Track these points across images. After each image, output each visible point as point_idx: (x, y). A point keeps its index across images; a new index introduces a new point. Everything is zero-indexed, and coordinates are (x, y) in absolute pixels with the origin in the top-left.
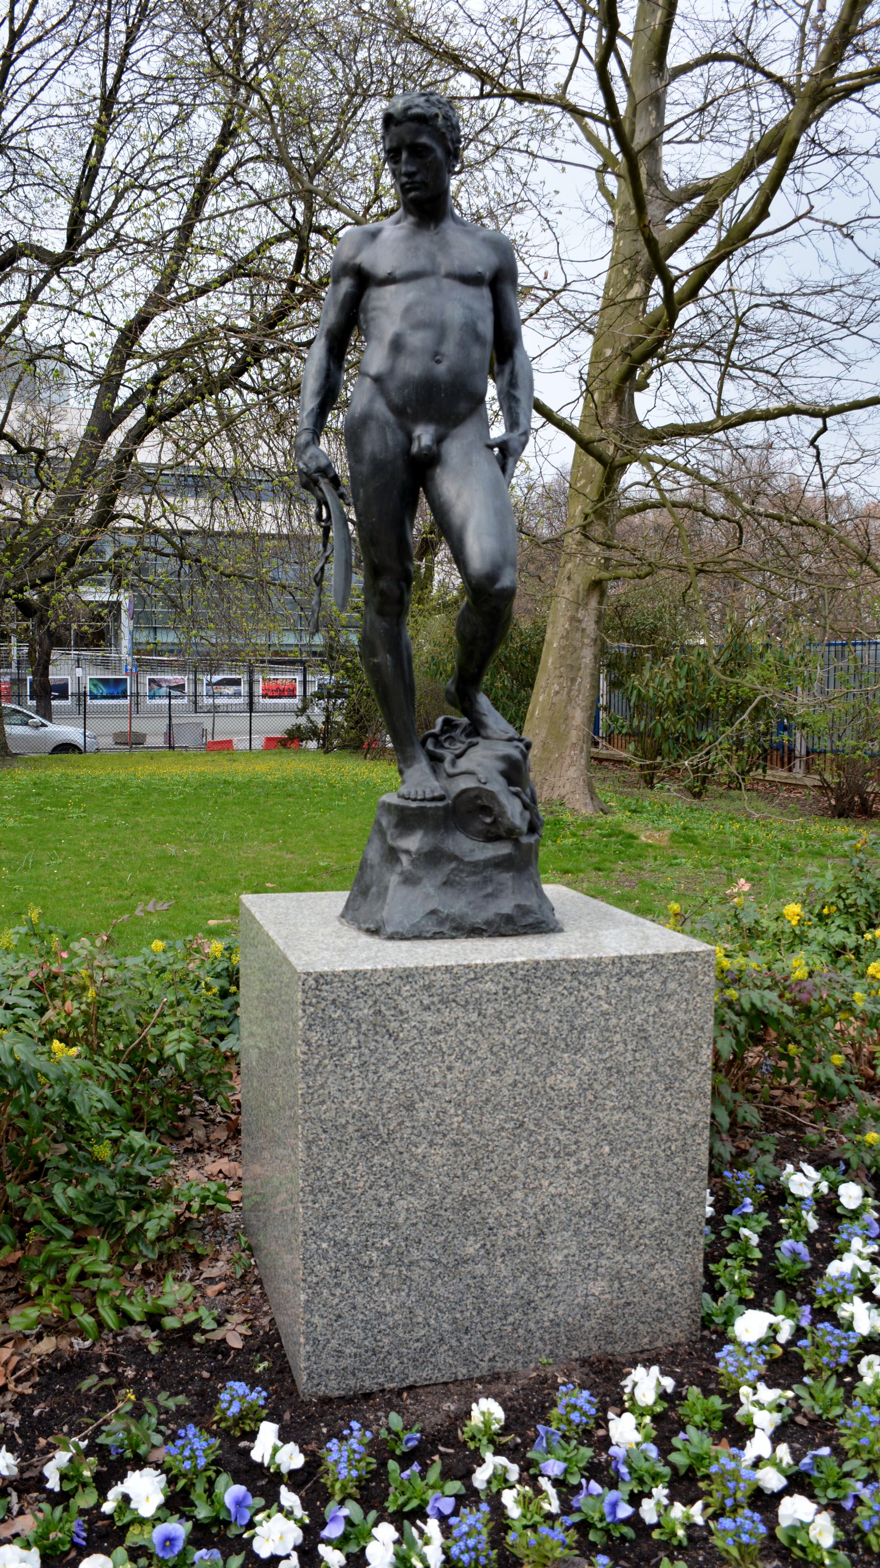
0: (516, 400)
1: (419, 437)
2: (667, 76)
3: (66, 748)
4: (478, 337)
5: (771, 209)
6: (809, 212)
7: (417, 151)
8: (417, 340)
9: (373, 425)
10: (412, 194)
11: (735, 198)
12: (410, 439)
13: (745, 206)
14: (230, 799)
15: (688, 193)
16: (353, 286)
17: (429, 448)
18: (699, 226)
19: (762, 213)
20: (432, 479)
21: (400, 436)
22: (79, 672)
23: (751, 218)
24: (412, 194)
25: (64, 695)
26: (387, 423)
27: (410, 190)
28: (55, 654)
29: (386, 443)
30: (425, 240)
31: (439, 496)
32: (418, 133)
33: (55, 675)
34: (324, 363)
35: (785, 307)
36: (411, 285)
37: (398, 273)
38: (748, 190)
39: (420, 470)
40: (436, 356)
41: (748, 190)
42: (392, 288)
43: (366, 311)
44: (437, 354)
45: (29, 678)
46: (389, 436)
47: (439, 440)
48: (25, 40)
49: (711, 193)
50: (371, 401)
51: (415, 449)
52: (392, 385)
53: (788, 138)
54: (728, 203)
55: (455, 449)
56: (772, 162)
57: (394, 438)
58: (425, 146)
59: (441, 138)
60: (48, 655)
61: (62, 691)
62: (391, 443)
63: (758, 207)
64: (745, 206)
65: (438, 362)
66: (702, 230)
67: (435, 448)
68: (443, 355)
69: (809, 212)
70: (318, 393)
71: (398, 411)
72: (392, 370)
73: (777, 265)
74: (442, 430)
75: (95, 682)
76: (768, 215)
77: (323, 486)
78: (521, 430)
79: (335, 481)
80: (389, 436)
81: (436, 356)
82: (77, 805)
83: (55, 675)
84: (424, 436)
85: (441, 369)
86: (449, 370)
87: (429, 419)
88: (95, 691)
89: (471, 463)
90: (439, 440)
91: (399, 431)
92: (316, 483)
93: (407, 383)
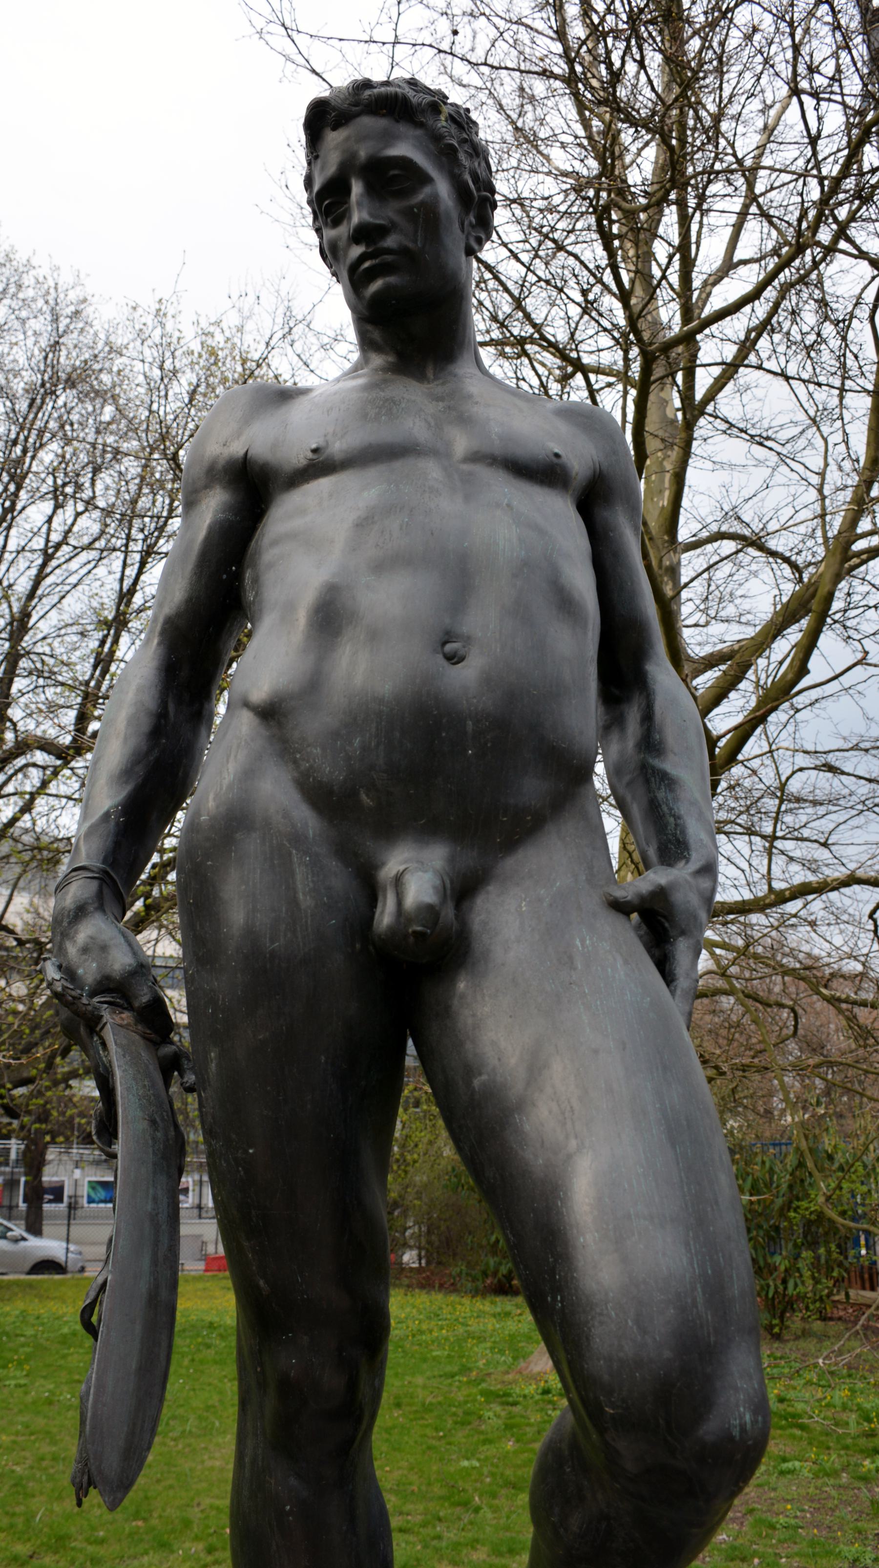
0: (667, 780)
1: (398, 881)
2: (679, 549)
3: (48, 1266)
4: (565, 603)
5: (811, 665)
6: (864, 658)
7: (389, 179)
8: (387, 599)
9: (252, 845)
10: (376, 286)
11: (768, 658)
12: (370, 889)
13: (781, 663)
14: (210, 1353)
15: (710, 662)
16: (228, 508)
17: (430, 912)
18: (729, 691)
19: (802, 670)
20: (446, 1013)
21: (340, 879)
22: (77, 1173)
23: (790, 676)
24: (376, 286)
25: (58, 1198)
26: (297, 839)
27: (371, 275)
28: (51, 1154)
29: (294, 902)
30: (411, 392)
31: (470, 1071)
32: (388, 138)
33: (49, 1177)
34: (150, 701)
35: (831, 769)
36: (373, 473)
37: (338, 448)
38: (783, 647)
39: (411, 979)
40: (449, 647)
41: (782, 647)
42: (323, 484)
43: (254, 565)
44: (448, 637)
45: (23, 1179)
46: (302, 878)
47: (463, 889)
48: (54, 563)
49: (737, 662)
50: (248, 774)
51: (385, 917)
52: (313, 726)
53: (823, 591)
54: (762, 662)
55: (510, 919)
56: (804, 623)
57: (319, 882)
58: (405, 163)
59: (447, 156)
60: (42, 1154)
61: (57, 1193)
62: (306, 901)
63: (797, 663)
64: (781, 663)
65: (454, 659)
66: (732, 695)
67: (449, 913)
68: (468, 640)
69: (864, 658)
70: (126, 773)
71: (328, 799)
72: (313, 685)
73: (821, 721)
74: (470, 859)
75: (93, 1185)
76: (808, 672)
77: (109, 1034)
78: (696, 861)
79: (154, 1019)
80: (302, 878)
81: (449, 647)
82: (20, 1364)
83: (49, 1177)
84: (414, 875)
85: (465, 679)
86: (487, 680)
87: (428, 826)
88: (93, 1194)
89: (567, 960)
90: (463, 889)
91: (333, 864)
92: (93, 1023)
93: (362, 716)
